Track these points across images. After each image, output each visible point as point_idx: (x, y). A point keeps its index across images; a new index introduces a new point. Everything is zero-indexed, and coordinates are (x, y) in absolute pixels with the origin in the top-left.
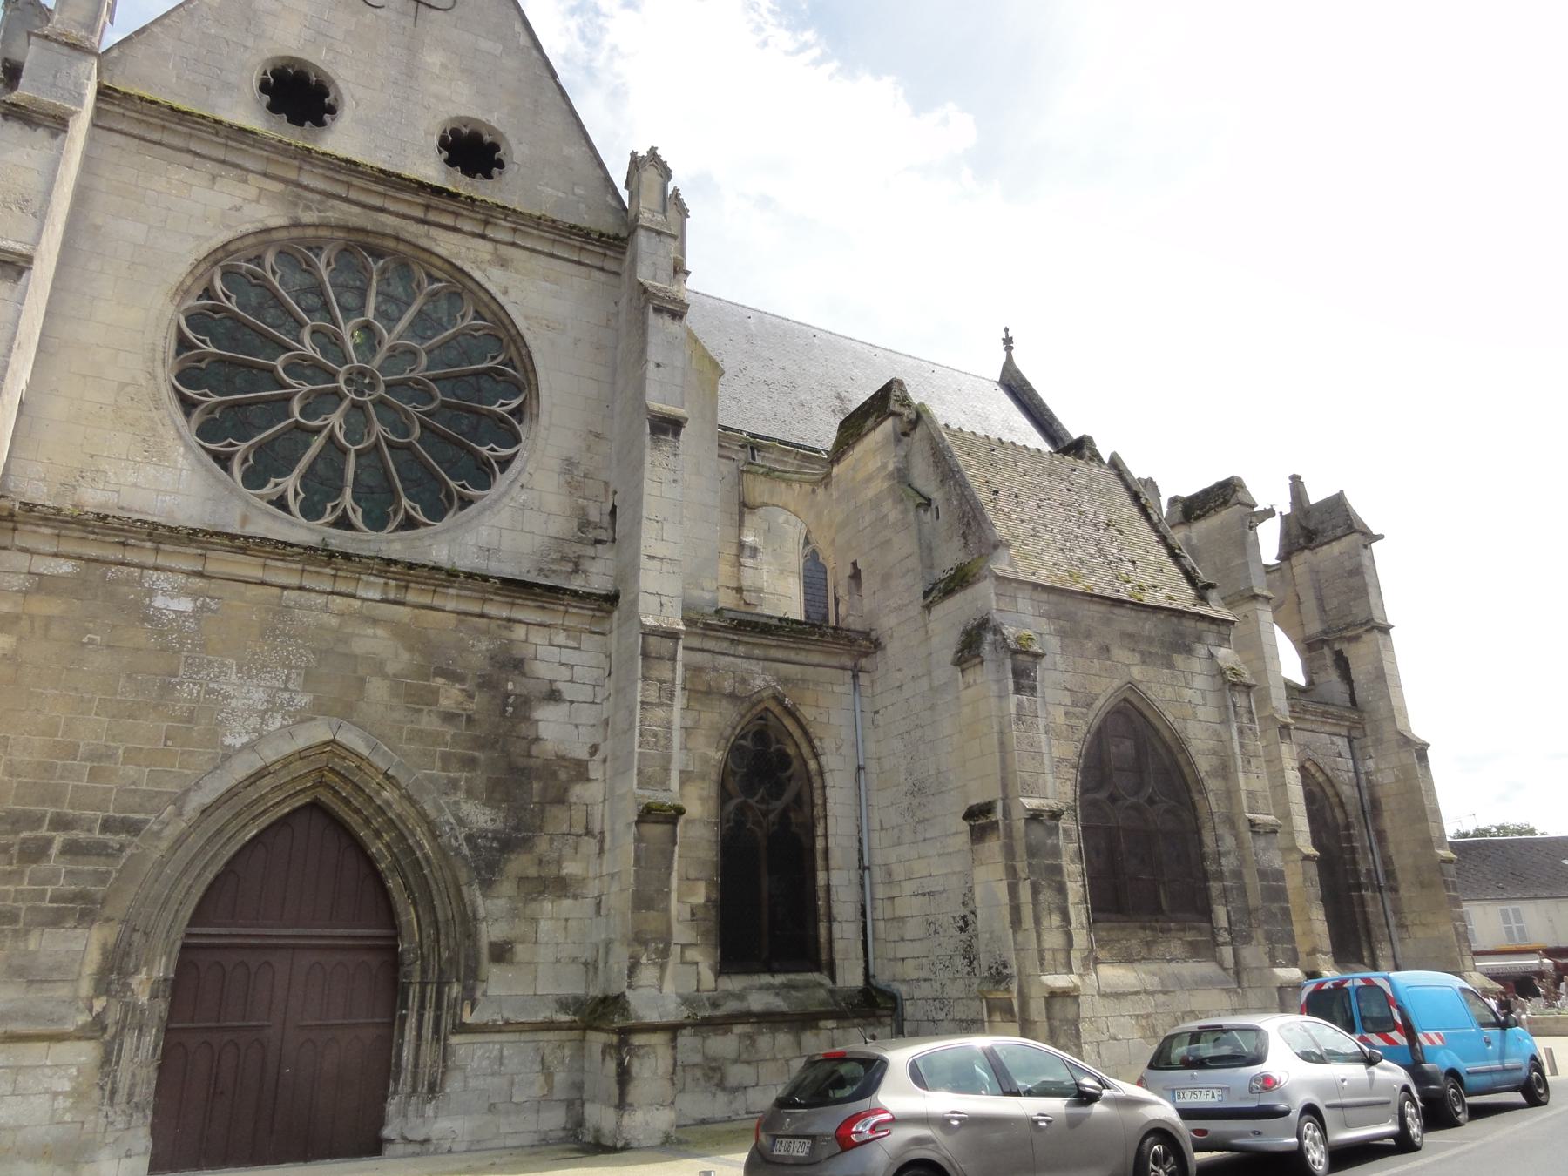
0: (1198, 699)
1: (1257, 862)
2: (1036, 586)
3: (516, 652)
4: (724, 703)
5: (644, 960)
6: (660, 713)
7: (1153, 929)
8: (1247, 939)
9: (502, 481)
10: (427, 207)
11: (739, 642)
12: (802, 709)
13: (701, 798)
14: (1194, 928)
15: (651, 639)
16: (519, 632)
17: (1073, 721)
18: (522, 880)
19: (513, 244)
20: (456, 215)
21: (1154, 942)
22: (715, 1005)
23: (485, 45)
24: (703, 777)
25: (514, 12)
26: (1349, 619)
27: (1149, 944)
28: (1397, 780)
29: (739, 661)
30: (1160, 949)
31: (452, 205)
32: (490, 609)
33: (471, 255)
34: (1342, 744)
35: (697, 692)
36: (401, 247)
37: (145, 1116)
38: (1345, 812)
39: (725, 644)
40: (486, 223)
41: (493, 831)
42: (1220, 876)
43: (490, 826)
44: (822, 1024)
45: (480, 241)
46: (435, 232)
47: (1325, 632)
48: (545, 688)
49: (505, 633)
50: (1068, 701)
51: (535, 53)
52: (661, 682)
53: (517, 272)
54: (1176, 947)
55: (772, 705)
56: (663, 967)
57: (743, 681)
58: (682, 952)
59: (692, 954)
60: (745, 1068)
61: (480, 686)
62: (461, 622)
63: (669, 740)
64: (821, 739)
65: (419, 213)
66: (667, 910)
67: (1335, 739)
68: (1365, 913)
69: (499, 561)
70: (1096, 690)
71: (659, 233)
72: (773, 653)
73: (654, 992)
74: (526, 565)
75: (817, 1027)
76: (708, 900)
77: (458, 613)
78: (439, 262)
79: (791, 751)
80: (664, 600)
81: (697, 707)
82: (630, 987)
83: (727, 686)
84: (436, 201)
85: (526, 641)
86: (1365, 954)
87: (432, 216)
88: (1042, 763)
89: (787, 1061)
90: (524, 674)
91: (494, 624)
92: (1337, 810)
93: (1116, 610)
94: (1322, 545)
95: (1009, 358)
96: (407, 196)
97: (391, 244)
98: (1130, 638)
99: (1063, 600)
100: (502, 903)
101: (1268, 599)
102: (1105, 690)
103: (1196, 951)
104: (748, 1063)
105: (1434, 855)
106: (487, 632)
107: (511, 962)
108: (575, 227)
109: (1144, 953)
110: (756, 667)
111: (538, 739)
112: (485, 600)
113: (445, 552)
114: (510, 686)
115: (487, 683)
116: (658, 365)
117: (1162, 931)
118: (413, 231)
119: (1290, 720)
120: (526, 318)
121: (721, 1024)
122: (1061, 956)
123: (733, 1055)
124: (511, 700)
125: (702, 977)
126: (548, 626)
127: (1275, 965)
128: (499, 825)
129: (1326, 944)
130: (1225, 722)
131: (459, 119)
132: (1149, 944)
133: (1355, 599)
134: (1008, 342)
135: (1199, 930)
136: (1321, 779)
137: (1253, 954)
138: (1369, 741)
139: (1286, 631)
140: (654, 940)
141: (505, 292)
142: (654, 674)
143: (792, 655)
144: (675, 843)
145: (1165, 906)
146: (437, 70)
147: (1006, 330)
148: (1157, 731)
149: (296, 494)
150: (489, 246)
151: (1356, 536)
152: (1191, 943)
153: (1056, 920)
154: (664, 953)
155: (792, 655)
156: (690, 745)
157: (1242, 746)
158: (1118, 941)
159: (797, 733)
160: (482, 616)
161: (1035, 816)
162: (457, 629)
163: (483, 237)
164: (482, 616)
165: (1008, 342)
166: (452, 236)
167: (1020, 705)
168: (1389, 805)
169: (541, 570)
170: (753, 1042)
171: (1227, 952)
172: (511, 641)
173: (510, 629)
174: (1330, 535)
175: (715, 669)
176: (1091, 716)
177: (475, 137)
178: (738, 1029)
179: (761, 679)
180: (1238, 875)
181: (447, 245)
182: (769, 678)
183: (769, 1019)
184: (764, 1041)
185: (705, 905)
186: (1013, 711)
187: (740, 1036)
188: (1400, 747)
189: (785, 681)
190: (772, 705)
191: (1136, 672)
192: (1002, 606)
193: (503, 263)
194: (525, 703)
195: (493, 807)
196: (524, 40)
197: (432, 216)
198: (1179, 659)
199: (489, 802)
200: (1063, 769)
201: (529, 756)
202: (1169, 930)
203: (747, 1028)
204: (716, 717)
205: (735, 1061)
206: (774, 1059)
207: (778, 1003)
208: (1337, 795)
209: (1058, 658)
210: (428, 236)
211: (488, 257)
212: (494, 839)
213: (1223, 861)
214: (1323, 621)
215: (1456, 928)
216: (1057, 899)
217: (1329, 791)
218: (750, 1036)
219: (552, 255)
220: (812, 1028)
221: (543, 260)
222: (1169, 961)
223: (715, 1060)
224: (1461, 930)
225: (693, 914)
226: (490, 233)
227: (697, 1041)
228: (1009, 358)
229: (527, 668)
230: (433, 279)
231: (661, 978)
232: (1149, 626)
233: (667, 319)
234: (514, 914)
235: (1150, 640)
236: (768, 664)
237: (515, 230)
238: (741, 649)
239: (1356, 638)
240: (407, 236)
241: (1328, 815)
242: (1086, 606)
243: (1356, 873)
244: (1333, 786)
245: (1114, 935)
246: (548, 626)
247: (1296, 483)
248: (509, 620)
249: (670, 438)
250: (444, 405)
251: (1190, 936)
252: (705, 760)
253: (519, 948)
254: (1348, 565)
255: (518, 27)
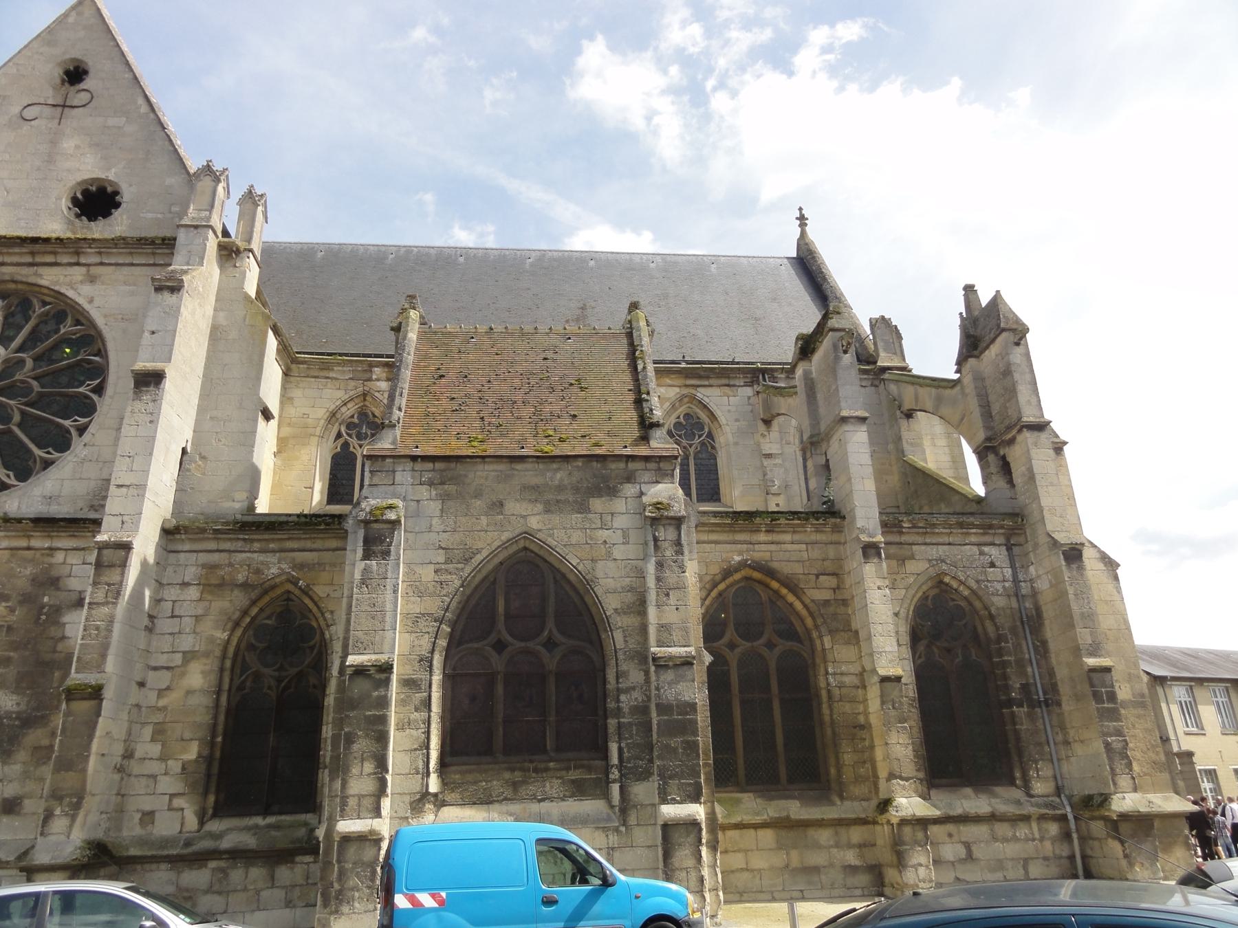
0: (617, 537)
1: (658, 696)
2: (414, 458)
3: (54, 573)
4: (236, 592)
5: (58, 812)
6: (105, 610)
7: (522, 770)
8: (644, 775)
9: (77, 444)
10: (33, 254)
11: (252, 541)
12: (316, 589)
13: (202, 672)
14: (582, 766)
15: (105, 552)
16: (59, 557)
17: (443, 578)
18: (36, 749)
19: (102, 264)
20: (55, 253)
21: (524, 782)
22: (188, 844)
23: (112, 122)
24: (207, 654)
25: (139, 90)
26: (1007, 422)
27: (515, 785)
28: (1052, 586)
29: (255, 555)
30: (523, 791)
31: (49, 248)
32: (35, 543)
33: (68, 279)
34: (997, 553)
35: (209, 585)
36: (20, 286)
37: (1188, 846)
38: (995, 624)
39: (240, 544)
40: (78, 254)
41: (18, 713)
42: (618, 712)
43: (15, 708)
44: (298, 859)
45: (76, 268)
46: (41, 270)
47: (988, 439)
48: (74, 597)
49: (47, 559)
50: (441, 559)
51: (152, 115)
52: (109, 585)
53: (103, 284)
54: (553, 786)
55: (290, 587)
56: (73, 818)
57: (258, 572)
58: (170, 800)
59: (178, 802)
60: (217, 898)
61: (21, 603)
62: (12, 555)
63: (110, 631)
64: (332, 612)
65: (29, 259)
66: (84, 771)
67: (986, 549)
68: (1017, 732)
69: (59, 504)
70: (480, 545)
71: (196, 227)
72: (290, 544)
73: (63, 837)
74: (80, 504)
75: (293, 862)
76: (200, 755)
77: (11, 549)
78: (46, 291)
79: (314, 624)
80: (125, 518)
81: (209, 598)
82: (42, 834)
83: (241, 578)
84: (37, 247)
85: (64, 563)
86: (1018, 775)
87: (38, 259)
88: (383, 621)
89: (258, 892)
90: (58, 589)
91: (38, 554)
92: (988, 624)
93: (519, 466)
94: (987, 347)
95: (803, 234)
96: (17, 250)
97: (12, 286)
98: (533, 492)
99: (453, 465)
100: (17, 768)
101: (863, 420)
102: (489, 539)
103: (579, 790)
104: (219, 893)
105: (1082, 664)
106: (32, 560)
107: (18, 814)
108: (141, 239)
109: (508, 793)
110: (272, 558)
111: (64, 638)
112: (29, 537)
113: (16, 504)
114: (46, 599)
115: (27, 599)
116: (153, 333)
117: (536, 770)
118: (26, 274)
119: (879, 538)
120: (105, 316)
121: (199, 859)
122: (368, 802)
123: (204, 887)
124: (45, 610)
125: (187, 820)
126: (83, 549)
127: (664, 801)
128: (23, 707)
129: (909, 768)
130: (645, 559)
131: (85, 181)
132: (515, 785)
133: (1009, 400)
134: (802, 219)
135: (589, 769)
136: (966, 593)
137: (642, 791)
138: (1029, 547)
139: (969, 443)
140: (70, 796)
141: (91, 301)
142: (104, 579)
143: (309, 544)
144: (99, 715)
145: (549, 744)
146: (71, 152)
147: (800, 209)
148: (564, 576)
149: (8, 476)
150: (83, 270)
151: (1004, 335)
152: (573, 782)
153: (369, 767)
154: (77, 806)
155: (309, 544)
156: (198, 630)
157: (658, 579)
158: (475, 783)
159: (315, 610)
160: (29, 548)
161: (360, 671)
162: (9, 561)
163: (78, 264)
164: (29, 548)
165: (802, 219)
166: (55, 270)
167: (366, 570)
168: (1049, 613)
169: (92, 506)
170: (226, 875)
171: (615, 789)
172: (51, 565)
173: (52, 556)
174: (987, 339)
175: (230, 565)
176: (468, 569)
177: (102, 190)
178: (213, 864)
179: (274, 566)
180: (643, 710)
181: (49, 278)
182: (284, 566)
183: (238, 855)
184: (237, 875)
185: (196, 761)
186: (358, 576)
187: (213, 870)
188: (1051, 550)
189: (301, 567)
190: (290, 587)
191: (534, 523)
192: (376, 480)
193: (92, 279)
194: (57, 611)
195: (18, 694)
196: (144, 109)
197: (38, 259)
198: (597, 504)
199: (17, 690)
200: (422, 623)
201: (54, 651)
202: (547, 770)
203: (222, 864)
204: (226, 604)
205: (206, 892)
206: (245, 889)
207: (250, 841)
208: (986, 608)
209: (435, 521)
210: (36, 274)
211: (80, 278)
212: (17, 718)
213: (623, 697)
214: (987, 428)
215: (1108, 746)
216: (373, 747)
217: (978, 604)
218: (222, 870)
219: (132, 265)
220: (287, 862)
221: (126, 270)
222: (543, 800)
223: (187, 890)
224: (1117, 746)
225: (184, 768)
226: (83, 260)
227: (172, 875)
228: (803, 234)
229: (61, 584)
230: (45, 303)
231: (71, 826)
232: (560, 475)
233: (166, 294)
234: (26, 775)
235: (560, 488)
236: (283, 554)
237: (100, 253)
238: (257, 546)
239: (1012, 441)
240: (19, 278)
241: (980, 629)
242: (480, 467)
243: (1007, 688)
244: (979, 598)
245: (470, 777)
246: (83, 549)
247: (969, 290)
248: (51, 549)
249: (151, 388)
250: (41, 395)
251: (574, 775)
252: (211, 640)
253: (26, 802)
254: (1002, 367)
255: (141, 101)
